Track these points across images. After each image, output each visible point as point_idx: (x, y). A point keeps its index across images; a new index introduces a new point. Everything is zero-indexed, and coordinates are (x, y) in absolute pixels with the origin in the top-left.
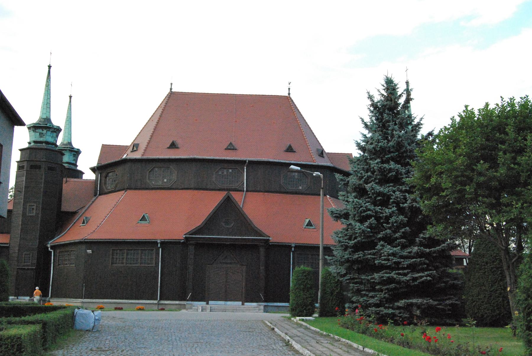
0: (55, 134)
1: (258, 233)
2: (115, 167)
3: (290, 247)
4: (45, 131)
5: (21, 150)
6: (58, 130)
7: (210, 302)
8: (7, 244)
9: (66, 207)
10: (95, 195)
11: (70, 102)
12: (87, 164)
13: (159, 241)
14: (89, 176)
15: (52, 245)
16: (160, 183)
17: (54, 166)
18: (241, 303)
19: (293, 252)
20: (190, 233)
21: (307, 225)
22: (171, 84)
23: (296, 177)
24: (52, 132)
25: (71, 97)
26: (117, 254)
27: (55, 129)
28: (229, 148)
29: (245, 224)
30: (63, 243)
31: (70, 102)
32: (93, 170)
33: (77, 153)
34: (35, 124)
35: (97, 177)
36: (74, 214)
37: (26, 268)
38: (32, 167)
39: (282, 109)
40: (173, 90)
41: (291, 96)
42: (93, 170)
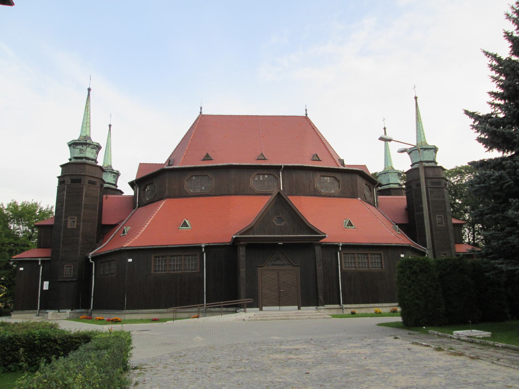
0: (94, 151)
1: (311, 230)
2: (154, 182)
3: (337, 246)
4: (85, 147)
5: (61, 166)
6: (98, 147)
7: (264, 308)
8: (49, 257)
9: (105, 221)
10: (134, 208)
11: (110, 130)
13: (203, 246)
14: (128, 192)
15: (93, 256)
16: (198, 191)
17: (95, 180)
18: (296, 307)
19: (340, 252)
20: (241, 232)
21: (348, 226)
22: (201, 108)
23: (329, 181)
24: (92, 148)
25: (110, 126)
26: (159, 260)
28: (260, 158)
29: (299, 221)
31: (110, 130)
32: (132, 184)
33: (117, 175)
34: (75, 141)
35: (135, 193)
36: (114, 226)
37: (67, 280)
38: (73, 181)
39: (302, 126)
40: (203, 113)
41: (308, 116)
42: (132, 184)
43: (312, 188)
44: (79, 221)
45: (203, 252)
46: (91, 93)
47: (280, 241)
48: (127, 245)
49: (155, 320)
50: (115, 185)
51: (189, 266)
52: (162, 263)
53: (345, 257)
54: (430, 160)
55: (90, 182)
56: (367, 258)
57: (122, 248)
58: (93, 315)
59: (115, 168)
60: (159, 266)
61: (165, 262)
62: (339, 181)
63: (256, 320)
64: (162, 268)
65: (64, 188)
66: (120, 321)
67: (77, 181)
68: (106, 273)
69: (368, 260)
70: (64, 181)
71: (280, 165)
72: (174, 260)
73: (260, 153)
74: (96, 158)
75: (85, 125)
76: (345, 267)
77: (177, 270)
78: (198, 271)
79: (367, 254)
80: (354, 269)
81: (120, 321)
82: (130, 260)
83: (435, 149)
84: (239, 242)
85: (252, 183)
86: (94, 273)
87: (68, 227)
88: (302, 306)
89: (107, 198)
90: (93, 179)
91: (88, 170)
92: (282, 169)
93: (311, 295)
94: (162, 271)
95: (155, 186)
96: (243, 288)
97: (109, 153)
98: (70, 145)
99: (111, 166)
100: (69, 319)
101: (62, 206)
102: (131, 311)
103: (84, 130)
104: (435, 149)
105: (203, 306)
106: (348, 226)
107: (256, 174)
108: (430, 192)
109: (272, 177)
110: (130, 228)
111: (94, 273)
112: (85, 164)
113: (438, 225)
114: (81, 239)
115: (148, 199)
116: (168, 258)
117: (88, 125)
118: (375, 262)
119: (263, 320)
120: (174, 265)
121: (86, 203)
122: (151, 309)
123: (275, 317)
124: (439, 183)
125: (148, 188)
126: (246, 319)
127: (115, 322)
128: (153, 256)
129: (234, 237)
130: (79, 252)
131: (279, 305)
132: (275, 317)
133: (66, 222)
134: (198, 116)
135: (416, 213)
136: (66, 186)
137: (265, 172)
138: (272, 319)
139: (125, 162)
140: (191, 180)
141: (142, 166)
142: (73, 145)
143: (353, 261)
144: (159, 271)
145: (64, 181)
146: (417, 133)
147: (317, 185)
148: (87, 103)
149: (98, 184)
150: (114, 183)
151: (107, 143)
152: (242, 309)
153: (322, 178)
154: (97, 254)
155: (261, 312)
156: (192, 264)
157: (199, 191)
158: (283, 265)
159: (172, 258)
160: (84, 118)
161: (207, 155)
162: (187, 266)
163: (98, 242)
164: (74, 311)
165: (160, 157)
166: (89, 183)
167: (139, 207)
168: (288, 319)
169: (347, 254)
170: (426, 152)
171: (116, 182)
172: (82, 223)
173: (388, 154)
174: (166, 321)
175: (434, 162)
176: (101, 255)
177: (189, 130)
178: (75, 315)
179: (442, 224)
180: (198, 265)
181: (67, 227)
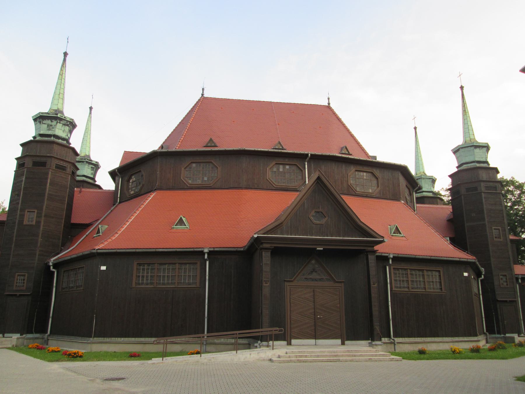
0: (67, 128)
1: (364, 231)
4: (54, 123)
7: (294, 341)
9: (76, 219)
13: (206, 250)
14: (107, 183)
15: (55, 262)
16: (199, 182)
21: (394, 233)
22: (203, 89)
24: (64, 125)
26: (143, 269)
27: (68, 121)
31: (90, 113)
32: (113, 174)
33: (96, 167)
34: (42, 113)
35: (117, 187)
36: (87, 226)
38: (35, 164)
39: (325, 116)
40: (205, 96)
41: (331, 105)
42: (113, 174)
43: (345, 185)
44: (39, 216)
45: (206, 260)
46: (67, 59)
47: (320, 245)
48: (101, 246)
49: (134, 356)
50: (93, 179)
51: (185, 279)
52: (148, 273)
53: (395, 274)
54: (481, 160)
55: (58, 167)
56: (423, 275)
57: (94, 251)
58: (50, 342)
59: (94, 158)
60: (143, 277)
61: (151, 272)
62: (377, 178)
63: (291, 361)
64: (147, 280)
65: (24, 172)
66: (81, 356)
68: (71, 285)
69: (424, 278)
70: (24, 164)
72: (164, 269)
73: (277, 142)
74: (69, 138)
75: (57, 96)
76: (397, 287)
78: (198, 285)
79: (422, 270)
80: (407, 290)
81: (81, 356)
82: (103, 268)
83: (486, 147)
84: (262, 243)
85: (269, 175)
86: (55, 285)
87: (24, 223)
88: (348, 339)
89: (80, 192)
91: (57, 151)
92: (308, 158)
93: (361, 323)
94: (147, 284)
95: (142, 176)
96: (266, 312)
97: (88, 141)
98: (35, 120)
99: (89, 156)
100: (16, 348)
101: (18, 195)
102: (101, 339)
103: (56, 102)
104: (486, 147)
105: (203, 337)
106: (394, 233)
107: (274, 163)
108: (485, 198)
109: (294, 168)
110: (107, 226)
111: (55, 285)
112: (53, 142)
113: (495, 239)
114: (40, 239)
115: (132, 192)
116: (156, 266)
117: (61, 96)
118: (433, 282)
119: (300, 361)
120: (164, 276)
123: (318, 356)
124: (476, 189)
125: (134, 178)
126: (274, 359)
127: (73, 357)
128: (135, 263)
129: (256, 236)
130: (37, 257)
131: (315, 337)
132: (318, 356)
133: (22, 216)
134: (199, 98)
135: (466, 225)
136: (26, 170)
137: (287, 161)
138: (315, 361)
139: (105, 146)
140: (190, 168)
141: (126, 154)
142: (39, 119)
143: (405, 279)
144: (142, 284)
145: (24, 164)
146: (464, 128)
147: (351, 182)
148: (61, 70)
149: (69, 170)
150: (92, 176)
151: (86, 129)
152: (265, 343)
153: (357, 173)
154: (60, 260)
155: (289, 347)
156: (189, 276)
157: (200, 183)
158: (321, 280)
159: (162, 267)
160: (56, 88)
161: (211, 140)
162: (184, 277)
163: (63, 245)
164: (24, 336)
165: (149, 142)
166: (56, 167)
167: (120, 202)
168: (339, 360)
169: (398, 269)
170: (477, 150)
171: (95, 175)
172: (43, 218)
173: (420, 158)
174: (150, 358)
175: (487, 162)
176: (65, 261)
177: (188, 113)
179: (499, 238)
180: (198, 277)
181: (23, 223)
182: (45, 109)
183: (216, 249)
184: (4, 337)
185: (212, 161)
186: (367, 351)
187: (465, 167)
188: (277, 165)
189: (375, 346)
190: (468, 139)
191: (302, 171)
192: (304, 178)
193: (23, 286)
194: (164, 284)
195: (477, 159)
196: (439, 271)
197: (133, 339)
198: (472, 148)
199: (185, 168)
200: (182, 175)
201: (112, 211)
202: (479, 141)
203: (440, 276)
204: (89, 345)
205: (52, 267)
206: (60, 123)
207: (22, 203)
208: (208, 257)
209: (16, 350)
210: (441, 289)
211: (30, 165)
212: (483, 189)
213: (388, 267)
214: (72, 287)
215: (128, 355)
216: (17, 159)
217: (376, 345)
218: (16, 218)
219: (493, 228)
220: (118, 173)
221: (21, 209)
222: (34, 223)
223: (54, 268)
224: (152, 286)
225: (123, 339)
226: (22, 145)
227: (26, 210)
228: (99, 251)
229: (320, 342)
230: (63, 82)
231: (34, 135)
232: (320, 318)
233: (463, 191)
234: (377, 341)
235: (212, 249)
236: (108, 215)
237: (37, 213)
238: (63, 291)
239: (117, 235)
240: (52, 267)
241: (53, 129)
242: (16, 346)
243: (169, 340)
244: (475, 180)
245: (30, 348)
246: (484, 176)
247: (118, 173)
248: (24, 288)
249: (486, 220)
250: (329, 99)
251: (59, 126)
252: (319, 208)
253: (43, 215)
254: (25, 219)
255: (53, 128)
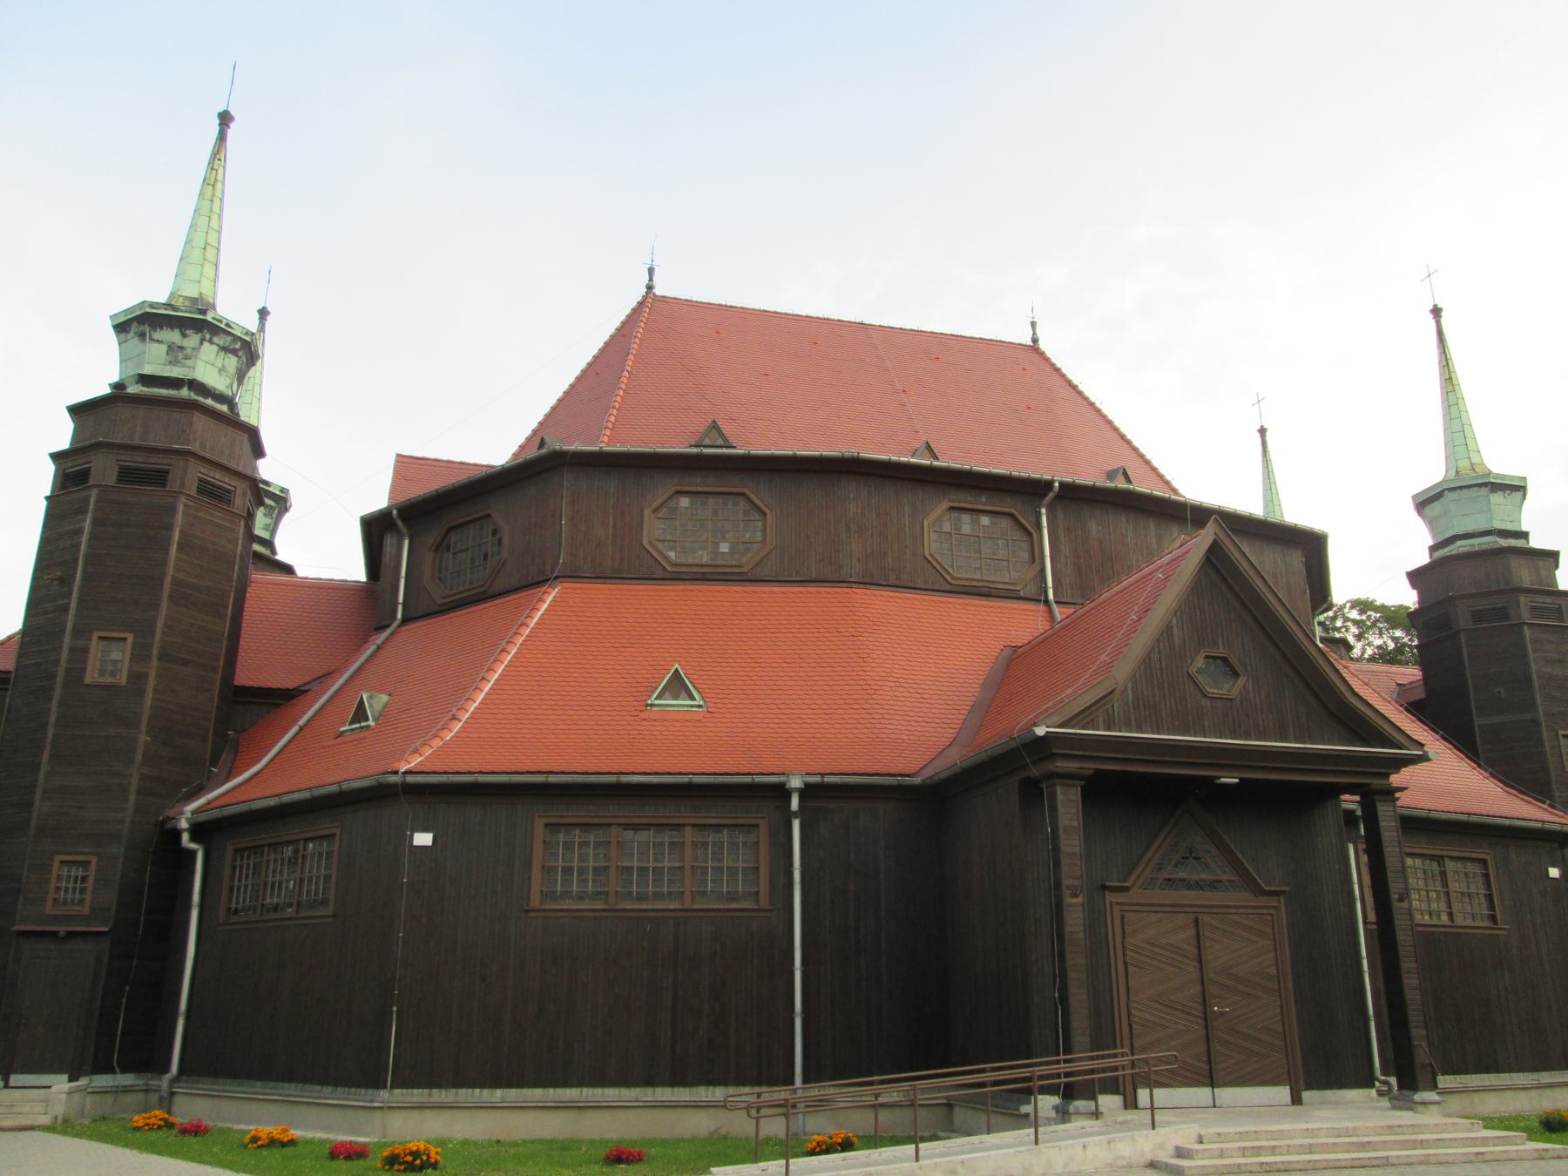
0: (232, 362)
2: (445, 531)
4: (193, 340)
12: (320, 542)
13: (796, 782)
15: (203, 817)
24: (224, 349)
26: (568, 845)
27: (236, 338)
30: (272, 802)
34: (152, 305)
38: (128, 475)
40: (658, 291)
41: (1042, 345)
48: (415, 762)
56: (1443, 874)
57: (393, 779)
60: (568, 870)
65: (87, 500)
67: (146, 474)
69: (1445, 884)
71: (1048, 477)
72: (719, 846)
75: (196, 255)
77: (658, 896)
82: (423, 839)
85: (932, 544)
86: (196, 897)
87: (88, 680)
88: (1310, 1086)
90: (217, 477)
92: (1051, 495)
98: (121, 328)
100: (64, 1126)
101: (65, 581)
102: (418, 1095)
103: (193, 272)
104: (1516, 489)
107: (945, 505)
108: (1534, 641)
109: (1005, 523)
110: (385, 698)
111: (196, 897)
121: (181, 576)
122: (520, 1085)
124: (1503, 613)
128: (539, 824)
130: (132, 797)
131: (1212, 1081)
133: (79, 654)
136: (94, 493)
137: (983, 501)
142: (139, 324)
144: (567, 895)
148: (211, 167)
157: (705, 560)
158: (1214, 885)
162: (710, 875)
164: (83, 1081)
165: (488, 433)
166: (200, 490)
167: (405, 620)
171: (273, 532)
172: (155, 662)
178: (89, 1099)
182: (158, 292)
183: (828, 779)
184: (6, 1086)
185: (748, 492)
186: (1438, 1128)
187: (1461, 546)
188: (955, 515)
189: (1420, 1108)
190: (1464, 464)
191: (1030, 535)
192: (1035, 556)
193: (81, 902)
194: (642, 897)
195: (1498, 525)
196: (1484, 862)
197: (537, 1093)
198: (1484, 491)
199: (655, 511)
200: (645, 533)
201: (379, 647)
202: (1495, 470)
203: (1487, 876)
204: (378, 1114)
205: (185, 837)
206: (211, 342)
207: (78, 609)
208: (800, 806)
209: (65, 1133)
210: (1493, 918)
211: (111, 478)
212: (1526, 615)
213: (1351, 848)
214: (276, 908)
215: (602, 1153)
216: (57, 457)
217: (1424, 1103)
218: (57, 662)
219: (1561, 732)
220: (399, 523)
221: (75, 630)
222: (123, 679)
223: (193, 839)
224: (599, 905)
225: (499, 1093)
226: (77, 411)
227: (95, 635)
228: (410, 779)
229: (1227, 1095)
230: (216, 209)
231: (116, 379)
232: (1222, 1014)
233: (1463, 620)
234: (1425, 1089)
235: (817, 779)
236: (367, 661)
237: (135, 646)
238: (267, 916)
239: (458, 726)
240: (185, 837)
241: (189, 362)
242: (65, 1121)
243: (765, 1097)
244: (1476, 588)
245: (137, 1129)
246: (1523, 575)
247: (399, 523)
248: (87, 910)
249: (1541, 709)
250: (1033, 324)
251: (209, 351)
252: (1215, 643)
253: (155, 652)
254: (89, 669)
255: (187, 358)
